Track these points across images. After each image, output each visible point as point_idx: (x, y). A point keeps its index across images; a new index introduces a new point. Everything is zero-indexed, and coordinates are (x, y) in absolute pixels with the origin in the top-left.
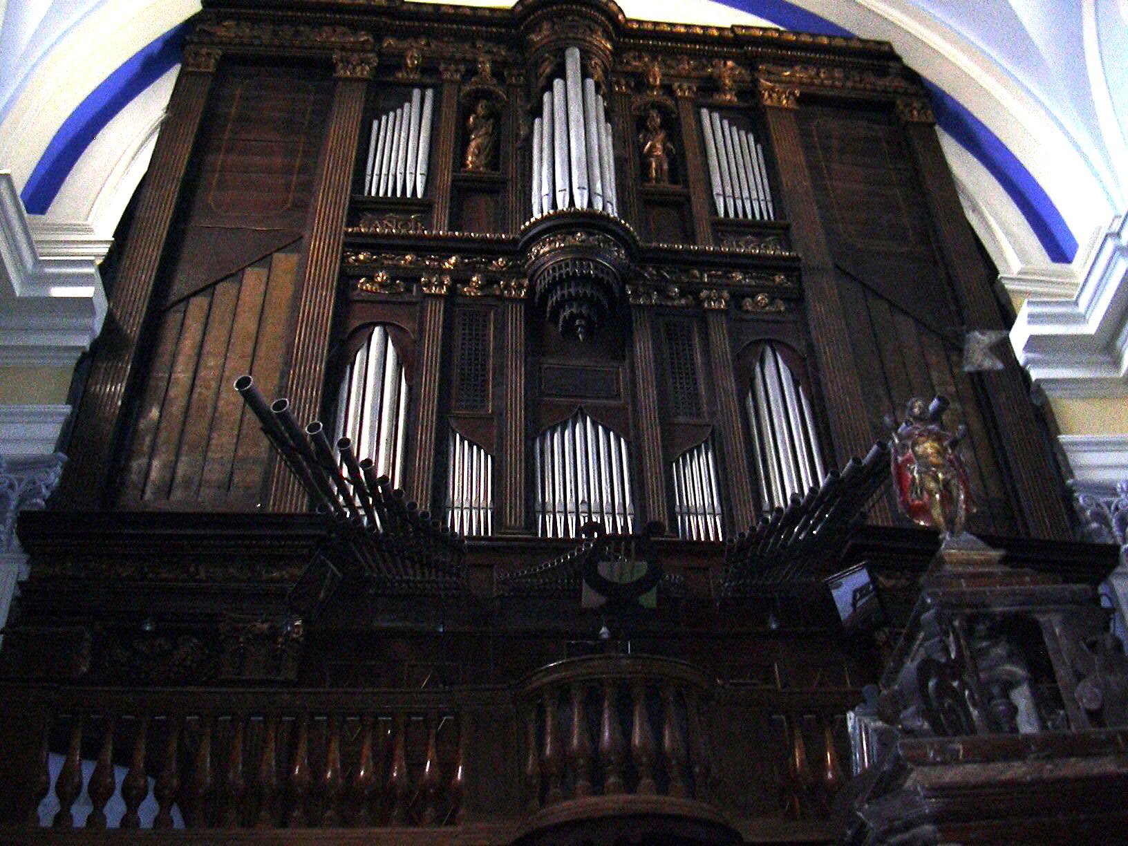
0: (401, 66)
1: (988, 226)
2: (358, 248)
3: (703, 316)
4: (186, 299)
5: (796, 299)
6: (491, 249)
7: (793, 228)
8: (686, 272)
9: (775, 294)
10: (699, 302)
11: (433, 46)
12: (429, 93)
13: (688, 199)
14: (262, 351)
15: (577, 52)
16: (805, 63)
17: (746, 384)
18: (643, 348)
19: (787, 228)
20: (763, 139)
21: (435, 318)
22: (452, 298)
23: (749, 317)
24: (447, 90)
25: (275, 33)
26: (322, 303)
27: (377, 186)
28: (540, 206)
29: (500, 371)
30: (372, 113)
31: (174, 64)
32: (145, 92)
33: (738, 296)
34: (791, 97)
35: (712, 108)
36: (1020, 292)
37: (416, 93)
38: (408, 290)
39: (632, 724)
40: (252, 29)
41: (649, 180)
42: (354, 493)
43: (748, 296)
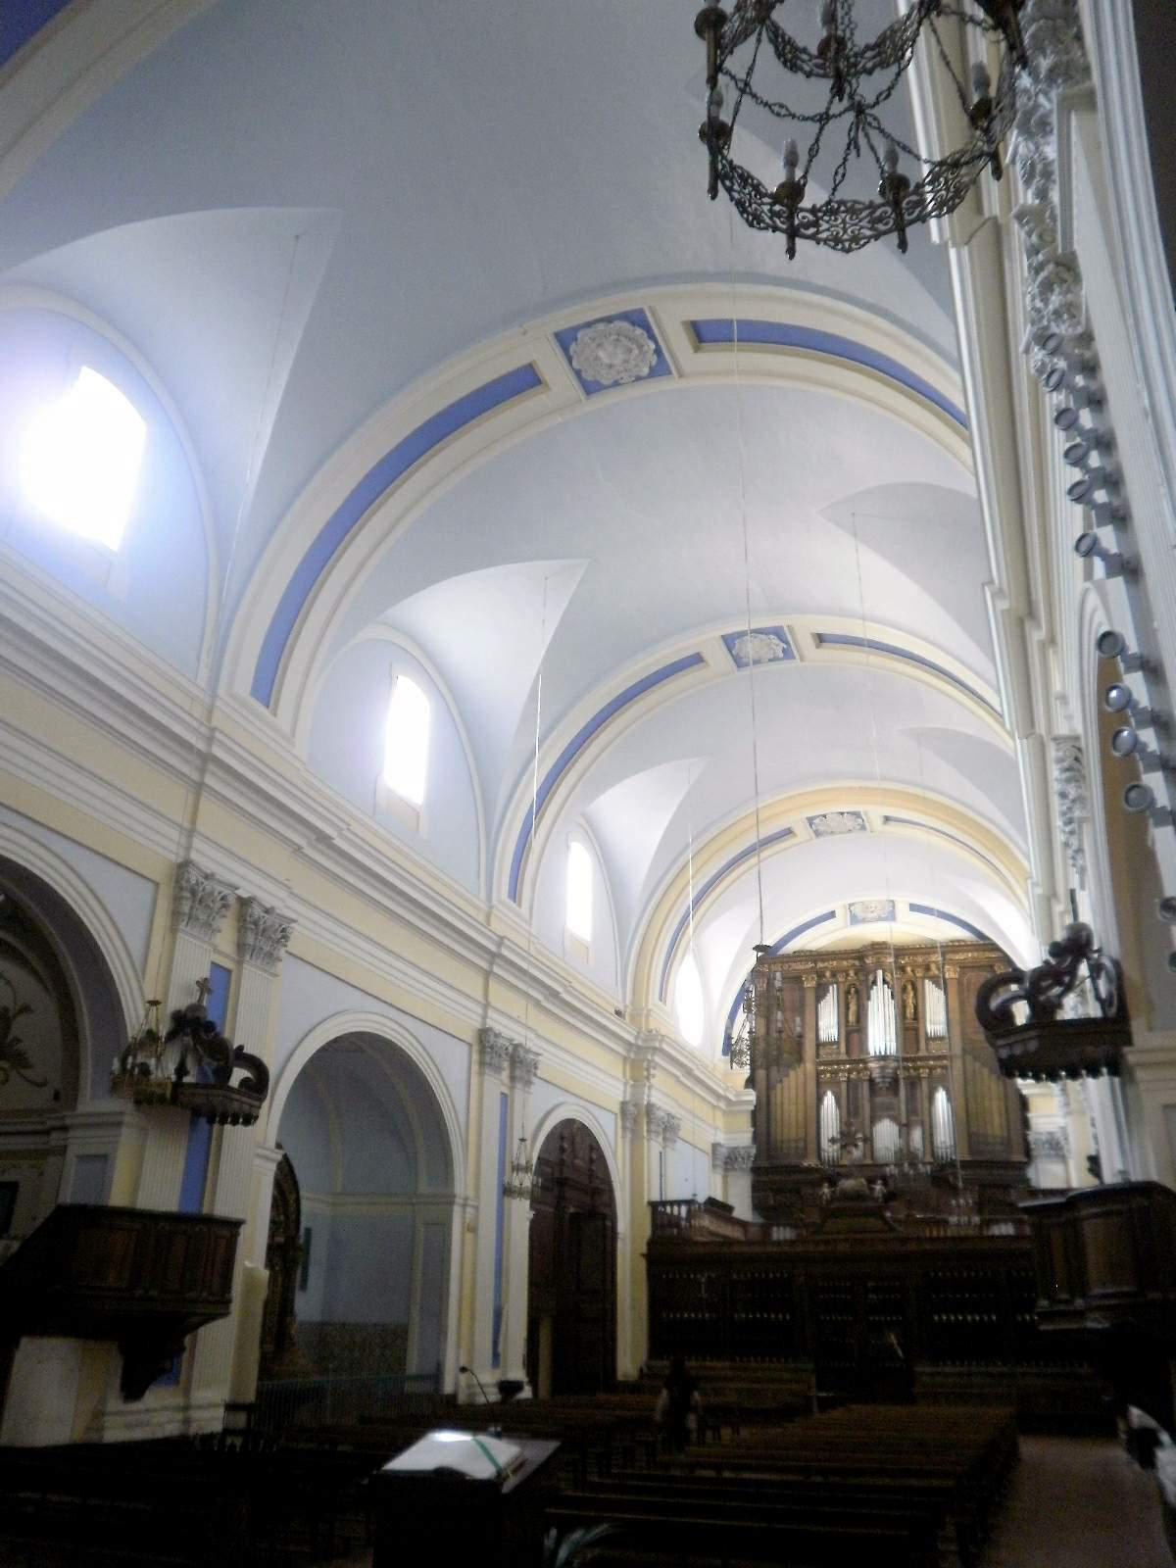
12: (835, 986)
17: (931, 1099)
21: (844, 1086)
22: (849, 1080)
24: (841, 986)
27: (823, 1036)
37: (831, 988)
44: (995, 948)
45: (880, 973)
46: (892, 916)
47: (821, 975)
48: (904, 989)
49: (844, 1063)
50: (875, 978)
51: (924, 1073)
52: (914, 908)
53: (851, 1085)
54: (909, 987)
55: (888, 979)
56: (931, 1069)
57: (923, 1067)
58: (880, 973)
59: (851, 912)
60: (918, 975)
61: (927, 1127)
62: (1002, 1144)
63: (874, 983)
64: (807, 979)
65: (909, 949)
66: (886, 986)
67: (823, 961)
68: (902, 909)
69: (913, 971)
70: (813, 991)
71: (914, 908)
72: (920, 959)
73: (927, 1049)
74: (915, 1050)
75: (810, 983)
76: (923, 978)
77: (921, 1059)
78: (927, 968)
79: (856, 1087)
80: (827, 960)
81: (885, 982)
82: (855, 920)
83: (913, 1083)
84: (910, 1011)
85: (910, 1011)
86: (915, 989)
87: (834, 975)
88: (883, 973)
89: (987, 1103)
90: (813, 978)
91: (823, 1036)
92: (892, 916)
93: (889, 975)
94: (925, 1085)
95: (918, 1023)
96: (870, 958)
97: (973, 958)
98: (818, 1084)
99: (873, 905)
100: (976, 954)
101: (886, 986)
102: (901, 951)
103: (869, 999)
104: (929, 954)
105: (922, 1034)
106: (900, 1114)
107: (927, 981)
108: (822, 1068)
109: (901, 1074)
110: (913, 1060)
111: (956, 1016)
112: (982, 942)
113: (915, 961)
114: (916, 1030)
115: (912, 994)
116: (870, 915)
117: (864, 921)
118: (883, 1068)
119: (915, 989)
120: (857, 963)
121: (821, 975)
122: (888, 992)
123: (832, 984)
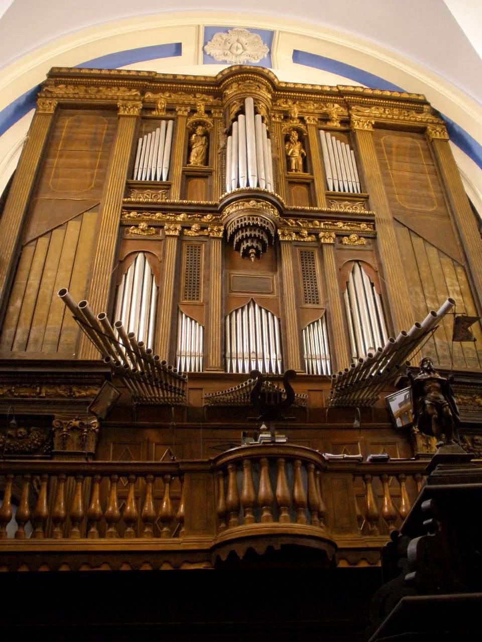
6: (203, 210)
8: (311, 222)
10: (318, 239)
12: (171, 122)
13: (313, 180)
15: (252, 100)
18: (288, 264)
20: (354, 146)
24: (181, 122)
25: (86, 91)
26: (109, 241)
27: (141, 175)
29: (208, 279)
30: (139, 134)
38: (157, 233)
41: (291, 170)
47: (148, 108)
49: (177, 210)
51: (328, 239)
53: (185, 245)
54: (295, 136)
59: (205, 52)
63: (242, 111)
67: (155, 91)
79: (195, 249)
98: (121, 240)
100: (396, 111)
103: (229, 133)
105: (319, 185)
106: (207, 303)
107: (322, 132)
108: (133, 214)
114: (309, 184)
121: (148, 108)
122: (263, 129)
123: (167, 119)
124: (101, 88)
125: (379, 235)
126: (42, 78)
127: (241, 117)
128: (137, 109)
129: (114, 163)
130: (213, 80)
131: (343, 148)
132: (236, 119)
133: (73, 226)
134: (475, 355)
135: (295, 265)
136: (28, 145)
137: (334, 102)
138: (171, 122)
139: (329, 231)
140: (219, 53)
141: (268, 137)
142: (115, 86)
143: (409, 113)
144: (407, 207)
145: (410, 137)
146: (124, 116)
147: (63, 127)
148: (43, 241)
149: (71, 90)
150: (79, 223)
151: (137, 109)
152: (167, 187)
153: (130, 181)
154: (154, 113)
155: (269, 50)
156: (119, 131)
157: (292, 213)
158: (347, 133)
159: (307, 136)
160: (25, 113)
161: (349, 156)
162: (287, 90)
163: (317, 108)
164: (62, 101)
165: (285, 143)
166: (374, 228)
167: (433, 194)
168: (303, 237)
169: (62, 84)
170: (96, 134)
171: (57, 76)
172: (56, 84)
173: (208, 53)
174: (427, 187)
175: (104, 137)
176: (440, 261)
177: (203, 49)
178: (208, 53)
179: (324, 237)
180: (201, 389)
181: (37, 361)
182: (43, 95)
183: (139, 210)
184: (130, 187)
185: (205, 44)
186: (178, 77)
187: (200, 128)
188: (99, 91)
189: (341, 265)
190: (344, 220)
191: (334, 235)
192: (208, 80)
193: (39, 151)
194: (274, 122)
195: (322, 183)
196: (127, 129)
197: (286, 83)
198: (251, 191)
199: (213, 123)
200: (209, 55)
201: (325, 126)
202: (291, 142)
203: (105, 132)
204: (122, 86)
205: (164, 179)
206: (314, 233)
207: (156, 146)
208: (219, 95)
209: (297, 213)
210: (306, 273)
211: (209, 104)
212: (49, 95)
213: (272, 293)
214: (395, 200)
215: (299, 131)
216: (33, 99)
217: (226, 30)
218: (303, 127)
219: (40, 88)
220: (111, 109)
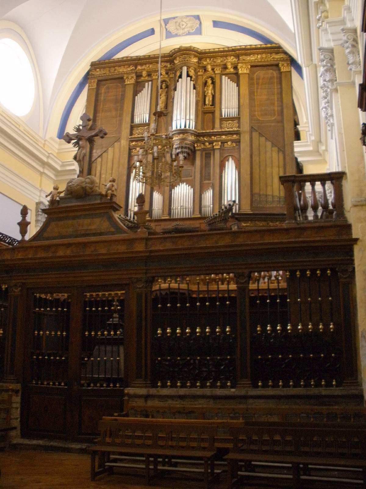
0: (141, 76)
1: (300, 106)
2: (132, 141)
3: (214, 150)
4: (96, 159)
5: (238, 142)
7: (241, 119)
8: (210, 137)
9: (233, 141)
11: (150, 67)
12: (150, 83)
13: (215, 111)
14: (114, 171)
16: (254, 54)
17: (222, 167)
18: (198, 162)
19: (239, 118)
20: (238, 85)
23: (226, 149)
25: (109, 71)
27: (137, 120)
28: (174, 128)
31: (86, 85)
32: (81, 95)
33: (223, 142)
34: (248, 69)
35: (226, 75)
36: (303, 130)
37: (147, 84)
39: (125, 367)
40: (104, 71)
41: (206, 105)
42: (225, 460)
43: (226, 143)
44: (278, 49)
45: (185, 69)
46: (199, 31)
47: (139, 76)
48: (205, 84)
50: (181, 73)
51: (217, 146)
52: (216, 24)
54: (210, 81)
55: (192, 73)
56: (223, 142)
57: (216, 141)
58: (185, 69)
59: (166, 29)
60: (216, 72)
61: (217, 189)
62: (279, 202)
63: (180, 77)
64: (127, 78)
65: (210, 53)
66: (189, 78)
67: (141, 65)
68: (207, 25)
69: (213, 69)
70: (132, 87)
71: (216, 24)
72: (219, 61)
73: (221, 128)
74: (212, 127)
75: (130, 81)
76: (222, 75)
77: (215, 134)
78: (225, 67)
80: (145, 64)
81: (188, 75)
82: (169, 35)
83: (208, 154)
84: (209, 100)
85: (209, 100)
86: (213, 83)
87: (149, 75)
88: (187, 69)
89: (269, 170)
90: (132, 77)
91: (137, 120)
92: (199, 31)
93: (193, 71)
94: (217, 154)
95: (214, 108)
96: (178, 58)
97: (262, 58)
99: (184, 23)
100: (264, 56)
101: (189, 78)
102: (202, 55)
103: (175, 89)
104: (226, 56)
108: (134, 143)
109: (198, 146)
110: (209, 135)
111: (246, 101)
112: (269, 45)
113: (215, 62)
114: (213, 113)
115: (211, 87)
116: (181, 32)
117: (177, 35)
118: (183, 139)
119: (213, 83)
120: (168, 65)
121: (139, 76)
123: (148, 81)
124: (116, 68)
125: (241, 141)
126: (88, 68)
127: (180, 79)
128: (133, 79)
129: (125, 114)
130: (168, 54)
131: (233, 86)
132: (178, 81)
133: (110, 150)
134: (278, 200)
135: (202, 162)
136: (88, 100)
137: (231, 56)
138: (150, 83)
139: (218, 141)
140: (174, 28)
141: (194, 88)
142: (122, 66)
143: (271, 55)
144: (261, 119)
145: (271, 70)
146: (127, 84)
147: (101, 94)
148: (99, 160)
149: (102, 72)
150: (113, 149)
151: (133, 79)
152: (148, 125)
153: (132, 124)
154: (142, 78)
155: (199, 22)
156: (126, 95)
157: (201, 134)
158: (236, 77)
159: (215, 81)
160: (83, 88)
161: (235, 89)
162: (205, 53)
163: (222, 61)
164: (100, 79)
165: (205, 87)
166: (240, 137)
167: (276, 108)
168: (206, 146)
169: (98, 68)
170: (116, 95)
171: (94, 65)
172: (95, 69)
173: (168, 30)
174: (273, 104)
175: (120, 96)
176: (272, 149)
177: (166, 28)
178: (168, 30)
179: (216, 145)
180: (160, 225)
181: (226, 28)
182: (90, 77)
183: (136, 141)
184: (132, 128)
185: (166, 25)
186: (151, 56)
187: (164, 83)
188: (115, 70)
189: (222, 159)
190: (225, 135)
191: (220, 143)
192: (166, 55)
193: (93, 105)
194: (199, 75)
195: (219, 112)
196: (129, 92)
197: (205, 50)
198: (183, 130)
199: (170, 81)
200: (169, 31)
201: (225, 72)
202: (208, 86)
203: (121, 93)
204: (125, 65)
205: (147, 122)
206: (211, 143)
207: (143, 100)
208: (172, 62)
209: (203, 134)
210: (206, 165)
211: (168, 68)
212: (93, 76)
213: (191, 177)
214: (255, 115)
215: (212, 79)
216: (87, 77)
217: (174, 18)
218: (213, 76)
219: (88, 73)
220: (121, 79)
